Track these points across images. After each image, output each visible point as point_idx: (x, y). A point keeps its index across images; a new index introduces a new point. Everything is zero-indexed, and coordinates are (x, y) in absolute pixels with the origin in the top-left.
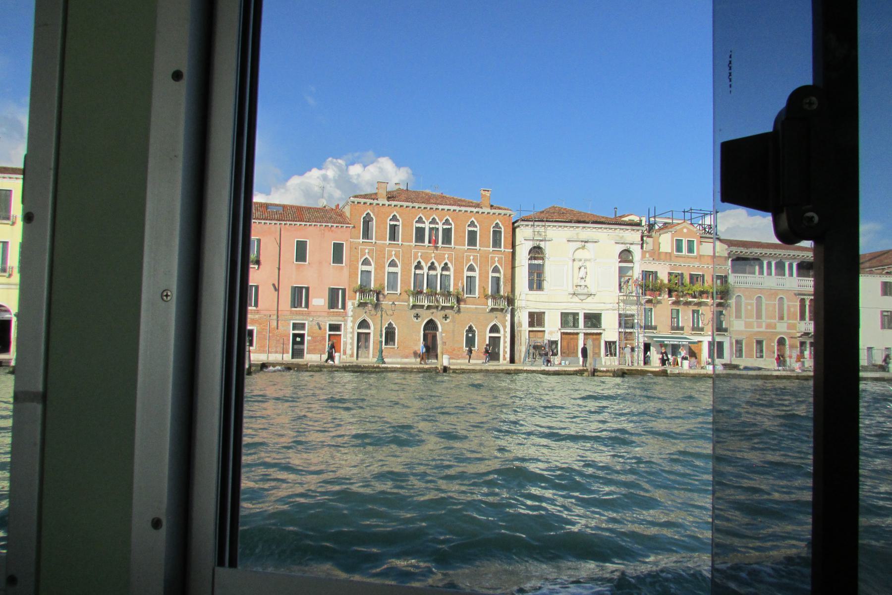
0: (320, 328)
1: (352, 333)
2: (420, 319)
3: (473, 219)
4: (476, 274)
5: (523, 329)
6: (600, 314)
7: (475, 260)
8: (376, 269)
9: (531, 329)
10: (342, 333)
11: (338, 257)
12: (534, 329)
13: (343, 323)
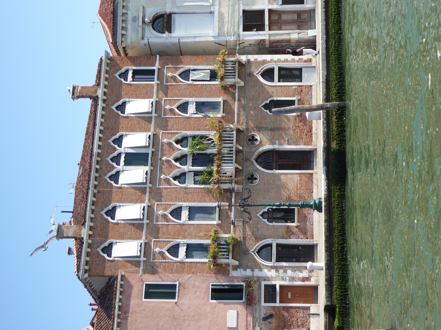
0: (271, 316)
1: (277, 268)
2: (256, 175)
3: (114, 107)
4: (296, 106)
5: (266, 37)
6: (244, 11)
7: (171, 102)
8: (184, 237)
9: (267, 28)
10: (278, 283)
11: (167, 292)
12: (236, 120)
13: (263, 283)
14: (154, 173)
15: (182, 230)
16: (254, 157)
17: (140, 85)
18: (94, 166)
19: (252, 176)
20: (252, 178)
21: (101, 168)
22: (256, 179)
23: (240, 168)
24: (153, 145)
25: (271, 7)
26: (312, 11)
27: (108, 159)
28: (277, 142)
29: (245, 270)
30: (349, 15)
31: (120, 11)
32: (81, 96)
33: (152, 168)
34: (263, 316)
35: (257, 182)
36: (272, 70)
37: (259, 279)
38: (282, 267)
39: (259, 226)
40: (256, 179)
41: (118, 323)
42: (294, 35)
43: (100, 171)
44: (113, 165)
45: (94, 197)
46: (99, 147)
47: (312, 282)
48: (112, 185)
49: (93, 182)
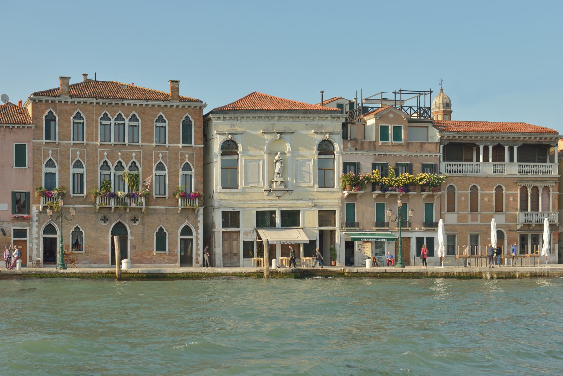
0: (4, 234)
2: (107, 223)
8: (60, 171)
9: (224, 230)
11: (20, 160)
13: (28, 229)
14: (108, 146)
15: (64, 169)
16: (121, 221)
17: (179, 133)
18: (150, 103)
19: (107, 220)
20: (105, 219)
21: (113, 107)
22: (105, 222)
23: (112, 211)
24: (131, 145)
25: (241, 233)
26: (237, 264)
27: (120, 112)
28: (133, 238)
29: (37, 215)
30: (72, 310)
31: (239, 115)
32: (172, 88)
33: (113, 145)
34: (4, 229)
35: (103, 223)
36: (191, 234)
37: (30, 226)
38: (39, 242)
39: (69, 225)
40: (105, 222)
41: (9, 127)
42: (218, 250)
43: (110, 106)
44: (115, 115)
45: (194, 107)
46: (129, 104)
47: (29, 263)
48: (71, 115)
49: (156, 103)
